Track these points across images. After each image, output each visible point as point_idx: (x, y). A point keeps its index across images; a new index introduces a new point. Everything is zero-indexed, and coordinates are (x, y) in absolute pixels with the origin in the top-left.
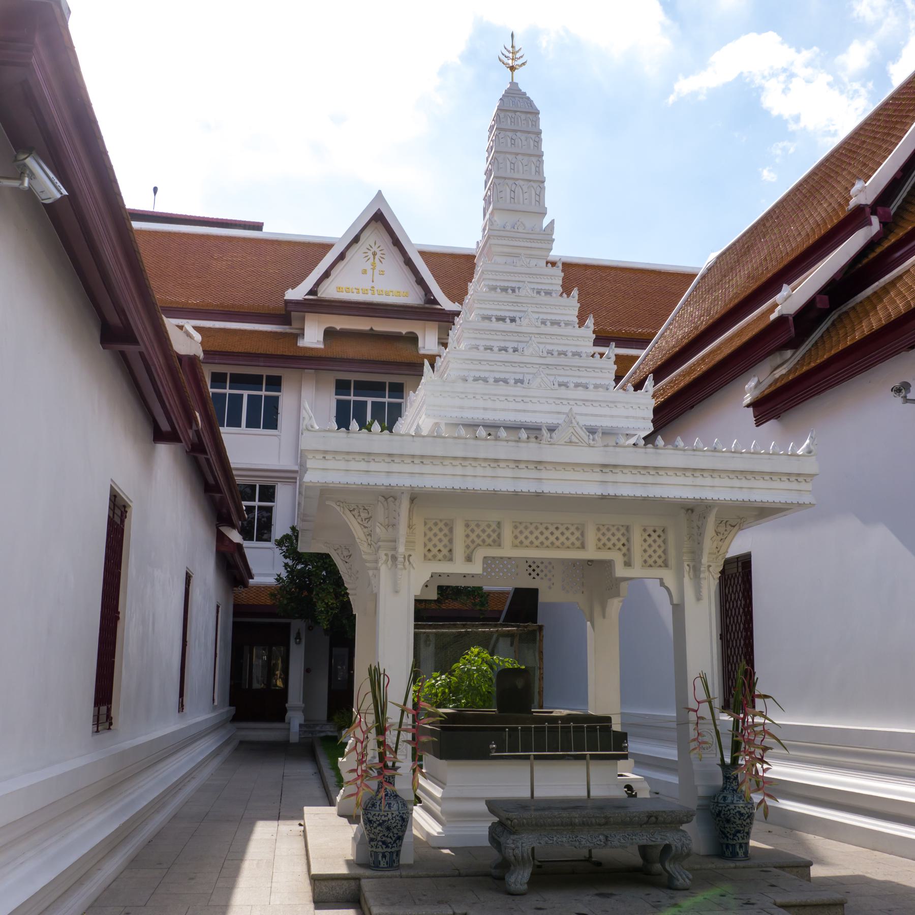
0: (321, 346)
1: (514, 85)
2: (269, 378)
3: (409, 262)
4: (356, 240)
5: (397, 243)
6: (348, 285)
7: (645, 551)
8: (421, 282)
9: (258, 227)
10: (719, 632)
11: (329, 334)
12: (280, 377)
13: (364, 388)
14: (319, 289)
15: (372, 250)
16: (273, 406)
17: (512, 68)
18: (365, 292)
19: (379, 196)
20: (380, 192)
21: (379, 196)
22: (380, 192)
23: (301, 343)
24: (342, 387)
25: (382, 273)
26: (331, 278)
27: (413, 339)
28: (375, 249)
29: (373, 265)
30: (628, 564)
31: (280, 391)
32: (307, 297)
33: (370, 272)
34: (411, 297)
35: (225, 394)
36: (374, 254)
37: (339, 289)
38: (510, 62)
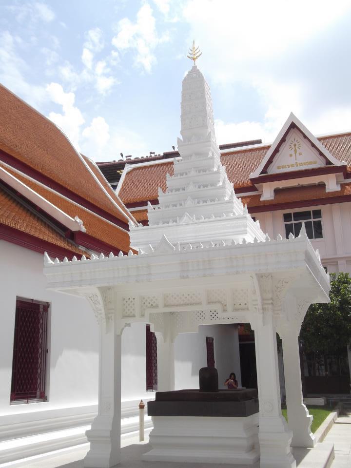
0: (273, 198)
1: (195, 67)
2: (314, 212)
3: (313, 145)
4: (283, 140)
5: (305, 137)
6: (287, 162)
7: (134, 310)
8: (321, 154)
9: (259, 142)
10: (48, 354)
11: (277, 191)
12: (320, 210)
13: (298, 216)
14: (267, 170)
15: (294, 144)
16: (318, 226)
17: (194, 59)
18: (293, 166)
19: (292, 115)
20: (292, 113)
21: (292, 115)
22: (292, 113)
23: (262, 199)
24: (287, 217)
25: (300, 154)
26: (319, 156)
27: (322, 186)
28: (295, 143)
29: (295, 151)
30: (225, 311)
31: (320, 217)
32: (260, 175)
33: (294, 155)
34: (320, 164)
35: (292, 224)
36: (295, 145)
37: (279, 168)
38: (193, 56)
